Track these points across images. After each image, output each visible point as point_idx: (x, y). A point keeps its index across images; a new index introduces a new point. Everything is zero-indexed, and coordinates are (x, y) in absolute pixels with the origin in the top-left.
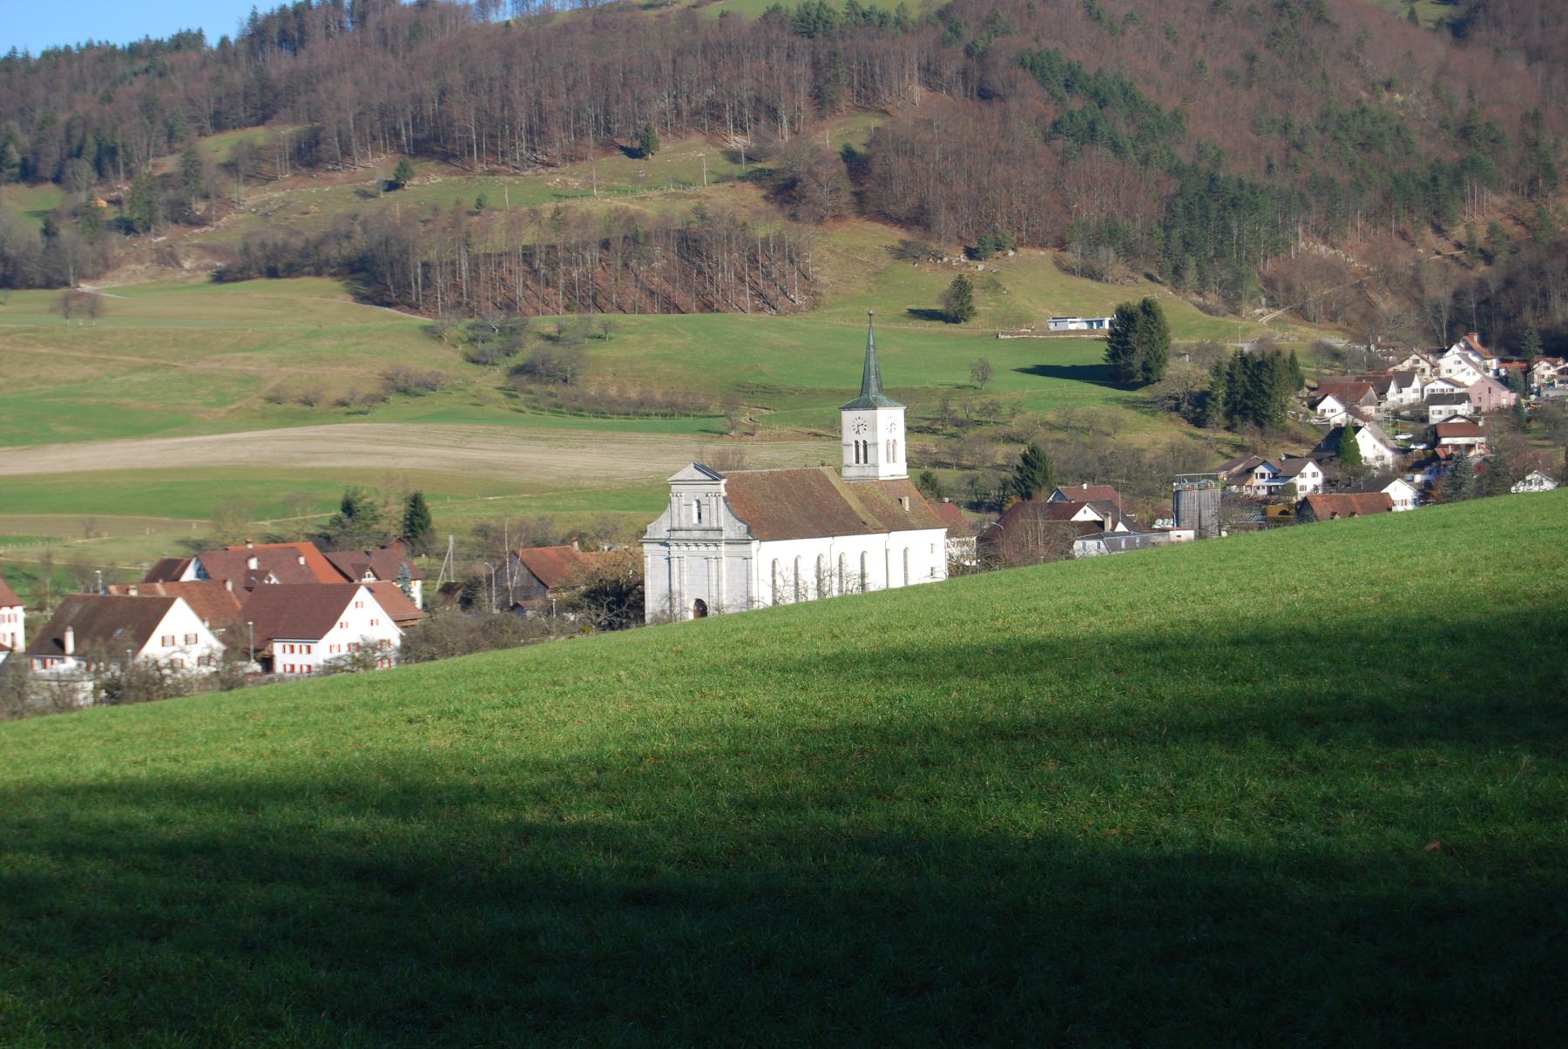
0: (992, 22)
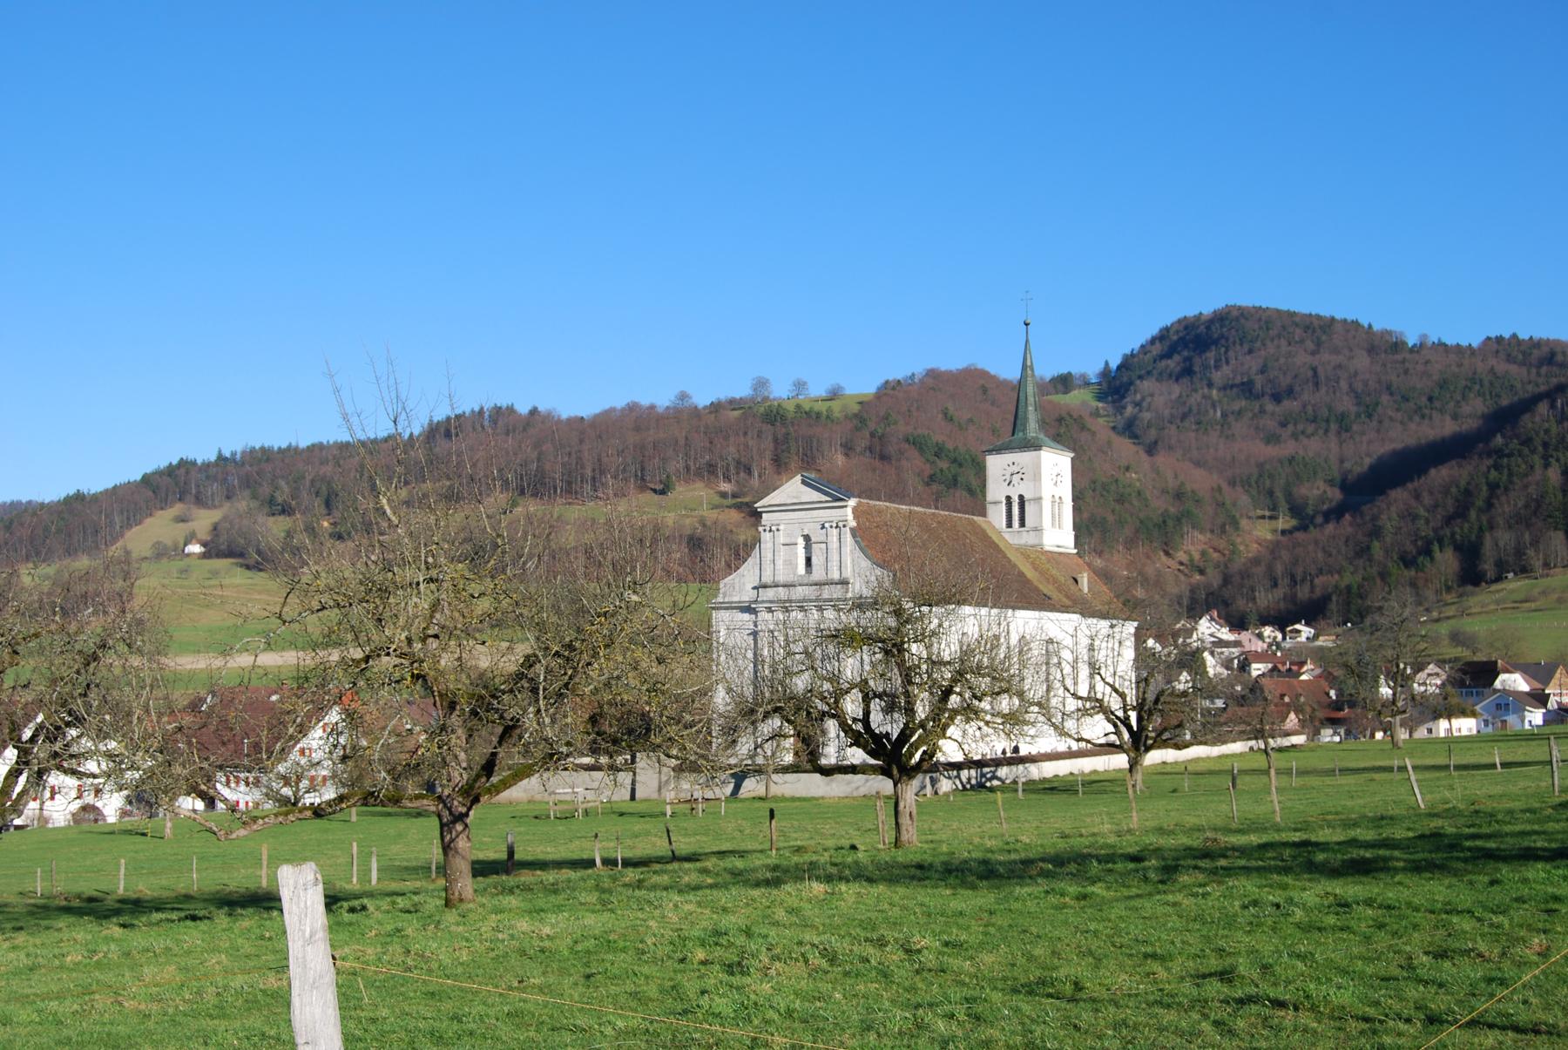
0: (887, 419)
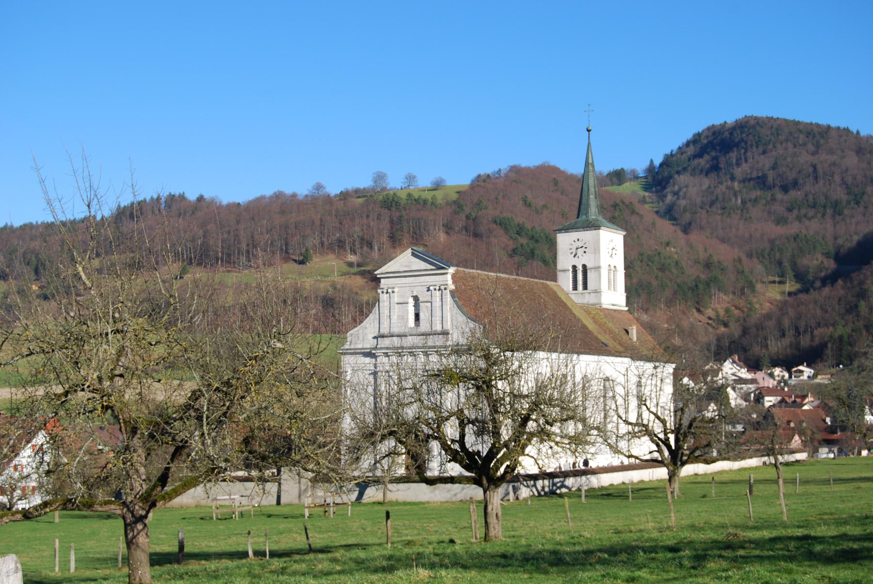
0: (479, 205)
